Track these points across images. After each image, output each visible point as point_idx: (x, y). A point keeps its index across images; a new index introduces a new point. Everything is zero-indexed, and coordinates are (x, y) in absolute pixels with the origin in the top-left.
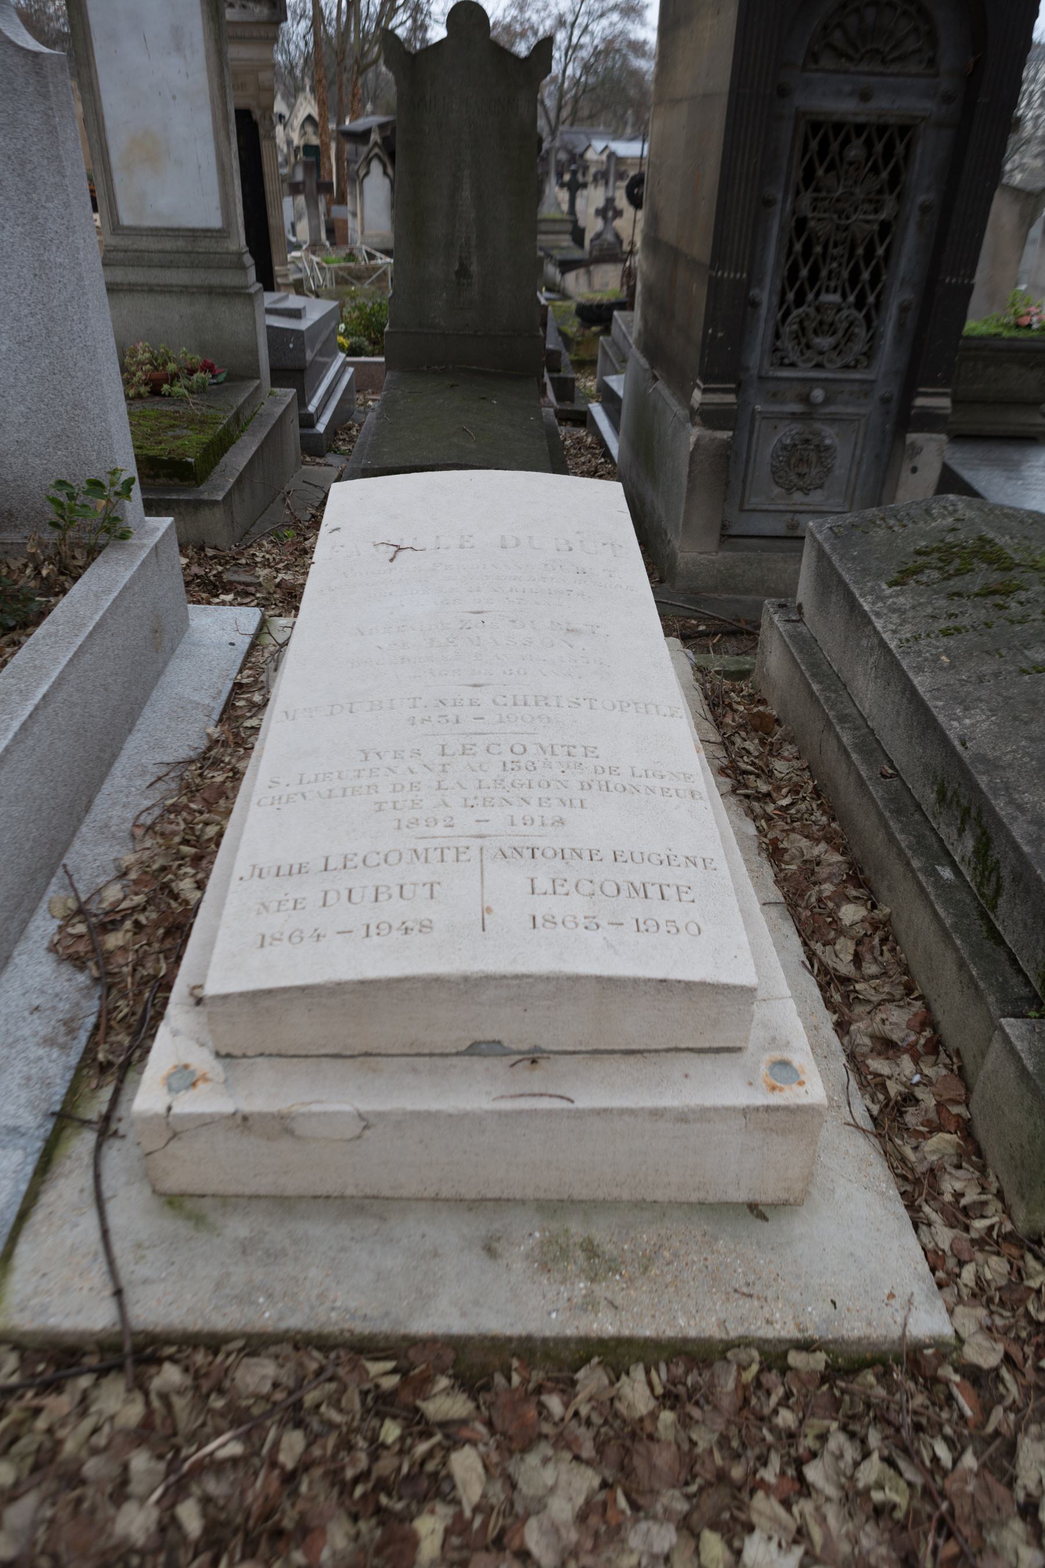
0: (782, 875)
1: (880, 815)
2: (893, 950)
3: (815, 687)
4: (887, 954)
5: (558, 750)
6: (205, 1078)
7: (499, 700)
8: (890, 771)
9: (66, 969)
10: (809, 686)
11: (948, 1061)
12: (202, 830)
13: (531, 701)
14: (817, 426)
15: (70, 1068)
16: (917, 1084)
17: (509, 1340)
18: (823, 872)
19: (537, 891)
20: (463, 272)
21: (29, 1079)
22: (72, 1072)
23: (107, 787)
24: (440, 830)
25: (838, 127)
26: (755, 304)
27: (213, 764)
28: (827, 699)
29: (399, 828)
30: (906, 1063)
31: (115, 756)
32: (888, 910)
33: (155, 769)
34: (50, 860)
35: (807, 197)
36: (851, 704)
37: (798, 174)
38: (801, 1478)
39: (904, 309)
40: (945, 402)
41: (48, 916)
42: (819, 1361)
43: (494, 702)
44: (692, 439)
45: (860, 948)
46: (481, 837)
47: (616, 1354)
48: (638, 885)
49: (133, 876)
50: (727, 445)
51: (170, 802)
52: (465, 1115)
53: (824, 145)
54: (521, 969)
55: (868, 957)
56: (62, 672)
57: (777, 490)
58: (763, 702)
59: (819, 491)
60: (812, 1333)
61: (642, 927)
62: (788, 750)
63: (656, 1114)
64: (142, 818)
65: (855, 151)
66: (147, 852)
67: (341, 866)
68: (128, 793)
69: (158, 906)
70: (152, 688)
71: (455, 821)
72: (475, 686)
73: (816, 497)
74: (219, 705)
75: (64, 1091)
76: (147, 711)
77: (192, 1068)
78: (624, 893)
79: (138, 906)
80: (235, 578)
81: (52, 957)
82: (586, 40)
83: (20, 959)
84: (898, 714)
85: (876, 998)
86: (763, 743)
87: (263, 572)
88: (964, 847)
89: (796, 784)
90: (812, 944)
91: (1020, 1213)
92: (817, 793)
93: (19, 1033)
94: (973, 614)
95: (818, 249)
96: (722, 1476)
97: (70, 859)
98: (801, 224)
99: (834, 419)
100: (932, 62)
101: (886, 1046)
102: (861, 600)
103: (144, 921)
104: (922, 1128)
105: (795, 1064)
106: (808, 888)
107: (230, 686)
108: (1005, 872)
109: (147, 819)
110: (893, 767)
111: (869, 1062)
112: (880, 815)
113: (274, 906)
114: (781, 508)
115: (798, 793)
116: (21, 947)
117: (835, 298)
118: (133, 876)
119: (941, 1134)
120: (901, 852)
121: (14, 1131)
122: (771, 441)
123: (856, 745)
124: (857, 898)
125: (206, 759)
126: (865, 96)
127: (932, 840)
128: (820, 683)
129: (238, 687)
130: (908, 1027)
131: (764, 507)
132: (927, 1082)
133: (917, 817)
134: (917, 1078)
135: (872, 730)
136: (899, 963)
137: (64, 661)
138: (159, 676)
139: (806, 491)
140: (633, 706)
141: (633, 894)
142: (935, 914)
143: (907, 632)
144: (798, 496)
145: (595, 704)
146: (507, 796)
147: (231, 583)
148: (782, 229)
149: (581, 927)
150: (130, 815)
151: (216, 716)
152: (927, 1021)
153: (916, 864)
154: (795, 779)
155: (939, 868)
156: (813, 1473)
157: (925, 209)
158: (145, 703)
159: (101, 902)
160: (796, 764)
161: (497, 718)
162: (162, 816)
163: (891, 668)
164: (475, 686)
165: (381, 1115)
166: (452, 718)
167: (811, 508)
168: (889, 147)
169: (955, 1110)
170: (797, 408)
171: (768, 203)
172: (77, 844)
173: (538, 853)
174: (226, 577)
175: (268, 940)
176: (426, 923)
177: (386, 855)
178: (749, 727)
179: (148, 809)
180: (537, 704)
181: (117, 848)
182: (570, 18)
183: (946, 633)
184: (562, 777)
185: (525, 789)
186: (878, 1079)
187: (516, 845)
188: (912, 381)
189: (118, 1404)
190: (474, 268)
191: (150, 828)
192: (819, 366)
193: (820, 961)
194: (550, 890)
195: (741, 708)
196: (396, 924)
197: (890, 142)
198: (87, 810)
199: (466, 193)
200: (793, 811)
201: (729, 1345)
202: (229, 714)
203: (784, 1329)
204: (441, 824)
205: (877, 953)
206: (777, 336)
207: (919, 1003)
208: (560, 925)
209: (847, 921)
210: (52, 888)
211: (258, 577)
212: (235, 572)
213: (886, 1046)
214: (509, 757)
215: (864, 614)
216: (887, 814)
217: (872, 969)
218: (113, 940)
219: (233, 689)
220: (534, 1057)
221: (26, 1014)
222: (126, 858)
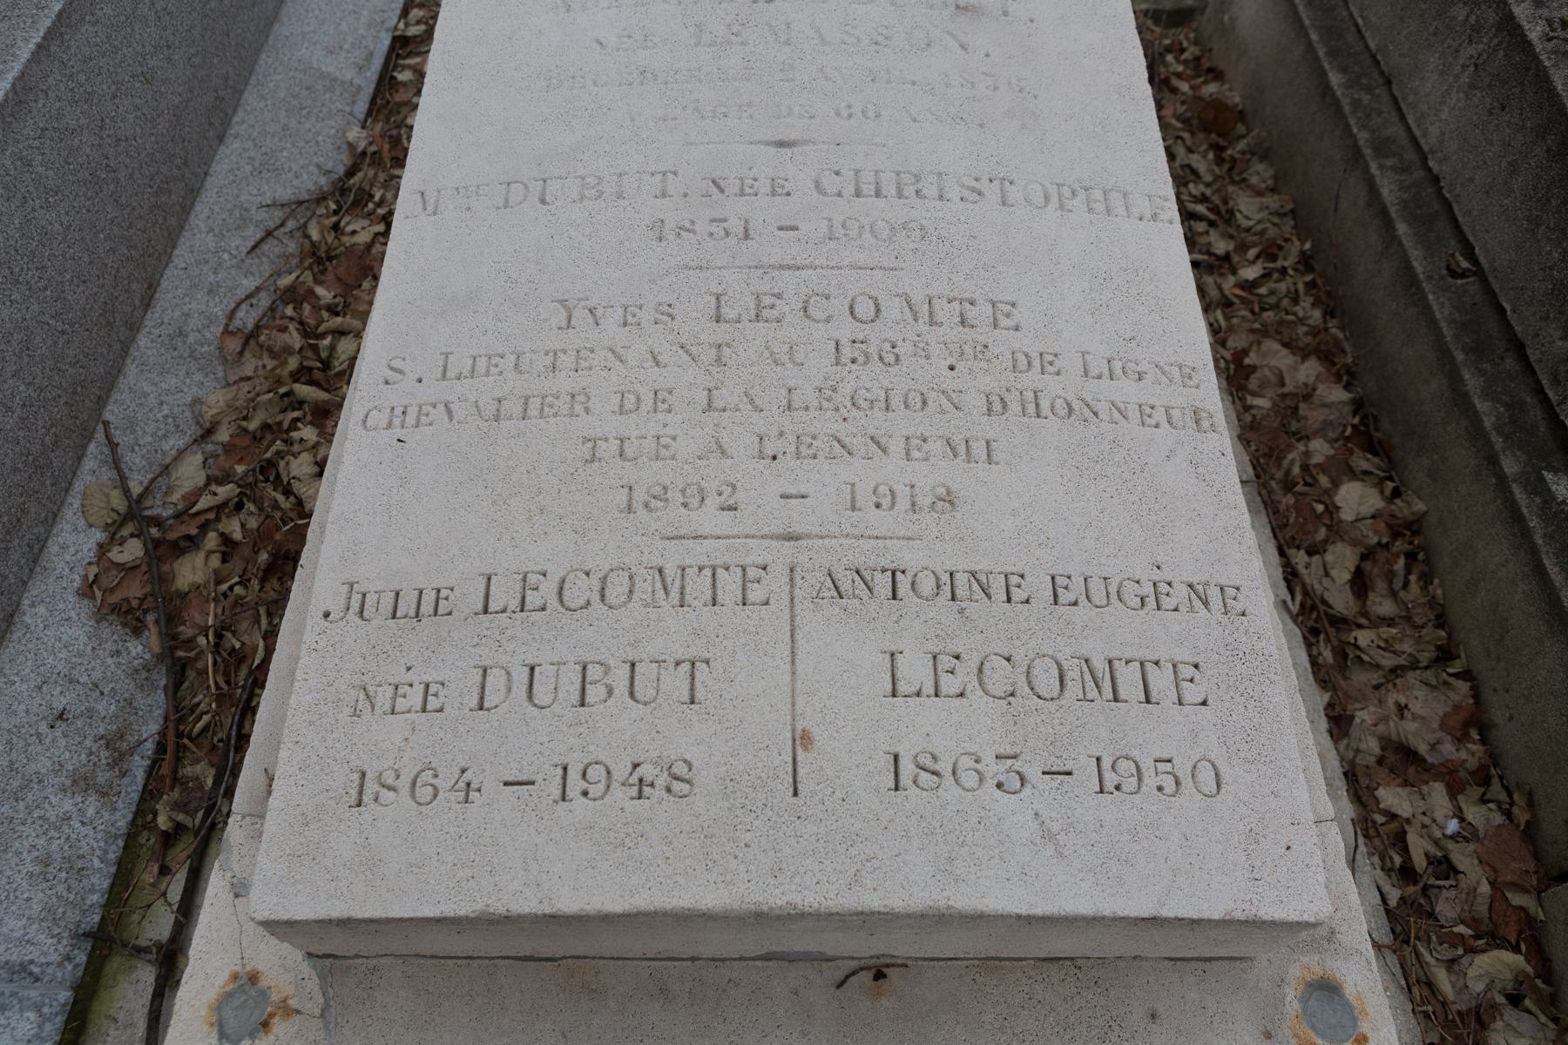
0: (1248, 418)
1: (1444, 354)
2: (1426, 579)
3: (1335, 79)
4: (1415, 588)
5: (944, 311)
6: (287, 1011)
7: (829, 182)
8: (1465, 264)
9: (112, 632)
10: (1323, 74)
11: (1503, 797)
12: (332, 348)
13: (889, 189)
15: (116, 837)
16: (1453, 837)
18: (1313, 416)
19: (903, 688)
21: (46, 862)
22: (121, 843)
23: (182, 255)
24: (709, 519)
27: (355, 204)
28: (1356, 104)
29: (629, 509)
30: (1438, 792)
31: (193, 194)
32: (1420, 507)
33: (262, 215)
34: (82, 412)
36: (1394, 118)
41: (82, 523)
43: (818, 184)
45: (1367, 566)
46: (792, 537)
48: (1100, 665)
49: (223, 435)
51: (286, 281)
54: (870, 900)
55: (1381, 585)
56: (22, 75)
58: (1216, 74)
61: (1110, 779)
62: (1260, 173)
64: (241, 314)
66: (246, 387)
67: (514, 603)
68: (215, 271)
69: (258, 502)
70: (258, 51)
71: (740, 496)
72: (781, 144)
75: (106, 884)
76: (250, 98)
77: (264, 983)
78: (1073, 689)
79: (225, 504)
81: (86, 607)
83: (33, 615)
84: (1513, 170)
85: (1388, 661)
86: (1219, 161)
89: (1272, 243)
90: (1291, 552)
92: (1306, 263)
93: (32, 768)
97: (111, 413)
101: (1403, 760)
103: (237, 535)
104: (1461, 929)
105: (1349, 991)
106: (1290, 448)
107: (387, 42)
109: (247, 318)
110: (1474, 260)
111: (1381, 793)
113: (384, 696)
115: (1273, 258)
116: (36, 589)
118: (223, 435)
119: (1496, 953)
120: (1477, 433)
121: (22, 972)
124: (1366, 473)
127: (1536, 414)
128: (1343, 70)
130: (1443, 726)
132: (1468, 834)
133: (1510, 363)
134: (1453, 826)
135: (1436, 180)
136: (1432, 603)
137: (25, 52)
138: (272, 24)
140: (1082, 195)
141: (1092, 693)
142: (1539, 570)
145: (1014, 194)
146: (842, 429)
149: (990, 783)
150: (219, 310)
151: (362, 107)
152: (1473, 722)
153: (1510, 466)
154: (1272, 232)
155: (1548, 476)
158: (246, 82)
159: (170, 490)
160: (1272, 201)
161: (824, 230)
162: (272, 309)
164: (781, 144)
166: (736, 225)
169: (1517, 899)
172: (131, 369)
173: (904, 583)
175: (371, 787)
176: (680, 769)
177: (604, 580)
178: (1195, 122)
179: (249, 297)
180: (900, 195)
181: (198, 377)
184: (949, 381)
185: (878, 413)
186: (1394, 825)
187: (860, 561)
191: (251, 336)
193: (1304, 585)
194: (929, 688)
195: (1184, 87)
196: (621, 771)
198: (147, 303)
200: (1263, 290)
204: (712, 502)
205: (1398, 583)
207: (1463, 686)
208: (948, 780)
209: (1347, 515)
210: (89, 464)
213: (1403, 760)
214: (845, 330)
216: (1460, 356)
217: (1386, 608)
218: (191, 571)
219: (392, 48)
221: (44, 728)
222: (212, 399)
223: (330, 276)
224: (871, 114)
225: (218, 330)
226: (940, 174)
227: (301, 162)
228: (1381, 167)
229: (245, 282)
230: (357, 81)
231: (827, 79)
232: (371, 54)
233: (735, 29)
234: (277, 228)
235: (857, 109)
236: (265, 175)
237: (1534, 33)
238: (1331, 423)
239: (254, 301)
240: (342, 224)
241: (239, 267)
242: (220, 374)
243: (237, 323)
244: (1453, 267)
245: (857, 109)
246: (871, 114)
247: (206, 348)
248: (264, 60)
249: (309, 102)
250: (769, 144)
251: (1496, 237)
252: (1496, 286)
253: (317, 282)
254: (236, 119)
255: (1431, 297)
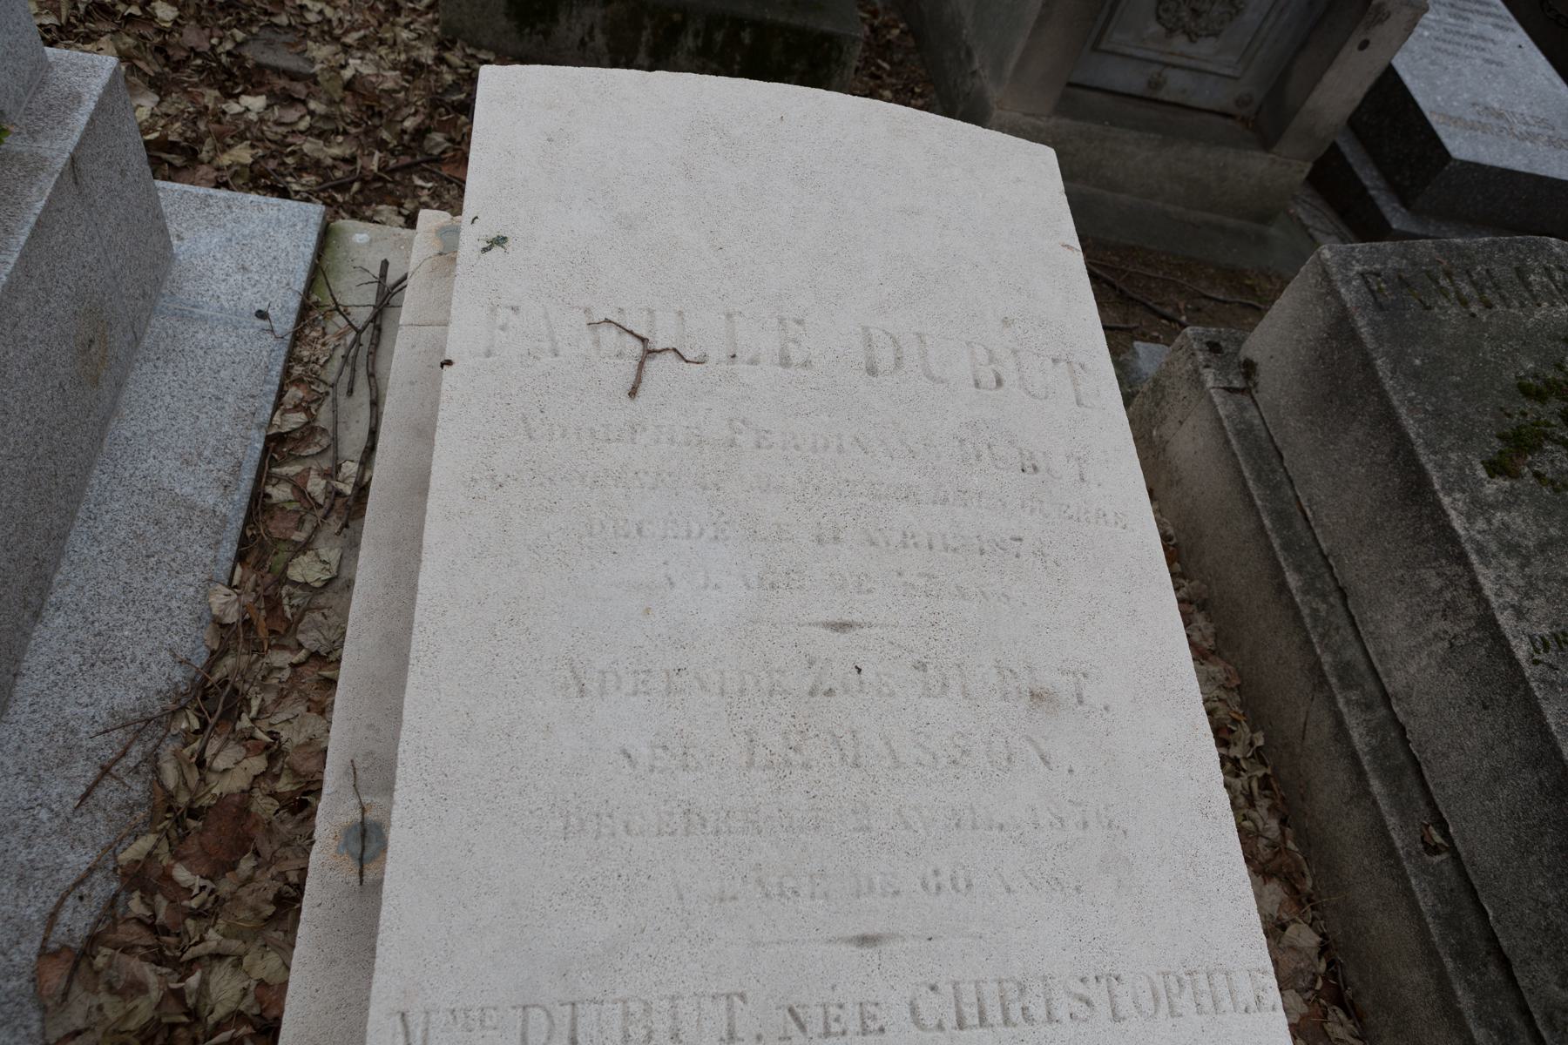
3: (1293, 580)
7: (931, 1007)
8: (1438, 839)
28: (1315, 612)
57: (1155, 28)
59: (1212, 40)
64: (65, 916)
72: (864, 940)
74: (234, 507)
80: (268, 58)
87: (322, 52)
102: (1446, 501)
109: (77, 922)
110: (1445, 834)
114: (1152, 55)
123: (1373, 751)
125: (213, 701)
128: (1299, 569)
129: (277, 446)
131: (1128, 51)
138: (106, 420)
139: (1192, 36)
147: (260, 67)
150: (33, 911)
151: (229, 549)
164: (864, 940)
167: (1193, 63)
174: (252, 54)
180: (1006, 1021)
202: (258, 541)
211: (312, 61)
212: (269, 43)
219: (266, 450)
223: (192, 846)
224: (962, 885)
225: (31, 947)
226: (1044, 978)
227: (149, 645)
228: (1348, 702)
229: (71, 857)
230: (222, 509)
231: (907, 827)
232: (240, 464)
233: (794, 739)
234: (116, 761)
235: (945, 879)
236: (100, 669)
237: (1522, 651)
238: (1302, 971)
239: (84, 890)
240: (208, 753)
241: (63, 833)
242: (35, 1027)
243: (59, 934)
244: (1427, 839)
245: (945, 879)
246: (962, 885)
247: (14, 983)
248: (97, 478)
249: (158, 546)
250: (849, 941)
251: (1482, 831)
252: (1476, 883)
253: (178, 857)
254: (58, 577)
255: (1413, 882)
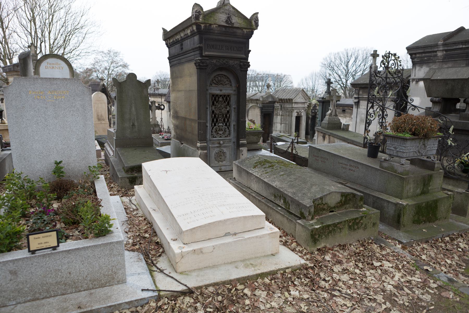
14: (222, 148)
17: (246, 277)
20: (133, 125)
25: (217, 95)
26: (207, 126)
35: (214, 107)
37: (211, 103)
38: (294, 284)
39: (234, 126)
40: (245, 141)
42: (290, 270)
44: (199, 153)
47: (262, 275)
50: (206, 153)
52: (229, 243)
53: (215, 98)
57: (216, 162)
60: (288, 266)
63: (257, 237)
65: (221, 99)
73: (224, 162)
82: (113, 72)
88: (281, 203)
91: (309, 249)
94: (269, 170)
95: (217, 116)
96: (284, 287)
98: (213, 112)
99: (225, 147)
100: (231, 85)
108: (290, 202)
112: (265, 204)
117: (222, 124)
122: (214, 152)
126: (221, 91)
139: (222, 162)
143: (260, 174)
144: (221, 163)
148: (210, 113)
153: (274, 208)
156: (295, 283)
157: (234, 108)
163: (259, 180)
165: (216, 245)
168: (226, 99)
170: (218, 145)
171: (207, 108)
182: (108, 68)
183: (266, 173)
188: (238, 139)
189: (188, 300)
190: (136, 124)
192: (221, 137)
197: (226, 98)
199: (133, 109)
201: (277, 271)
203: (284, 266)
206: (212, 132)
215: (251, 173)
220: (235, 234)
